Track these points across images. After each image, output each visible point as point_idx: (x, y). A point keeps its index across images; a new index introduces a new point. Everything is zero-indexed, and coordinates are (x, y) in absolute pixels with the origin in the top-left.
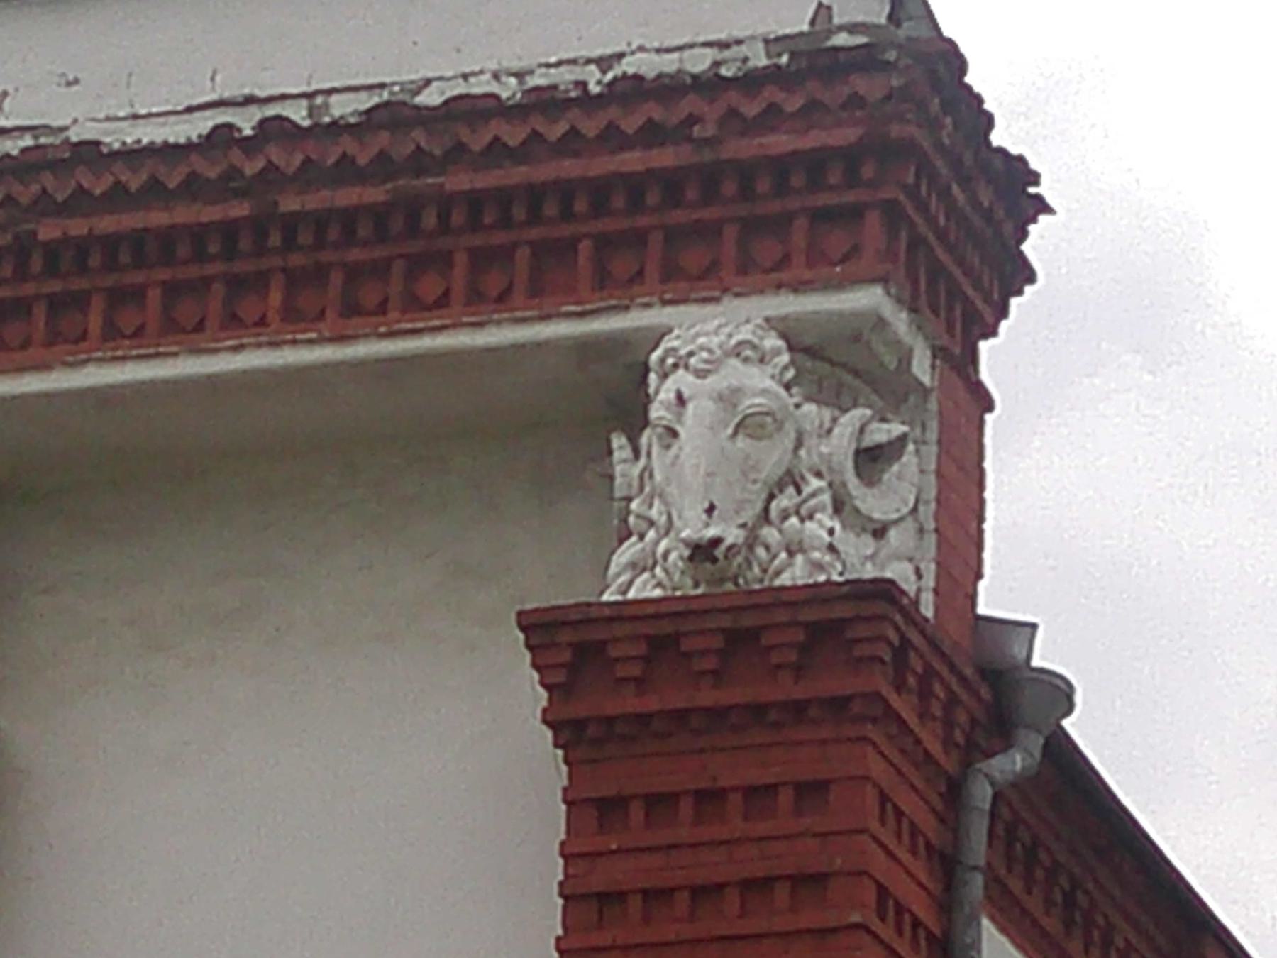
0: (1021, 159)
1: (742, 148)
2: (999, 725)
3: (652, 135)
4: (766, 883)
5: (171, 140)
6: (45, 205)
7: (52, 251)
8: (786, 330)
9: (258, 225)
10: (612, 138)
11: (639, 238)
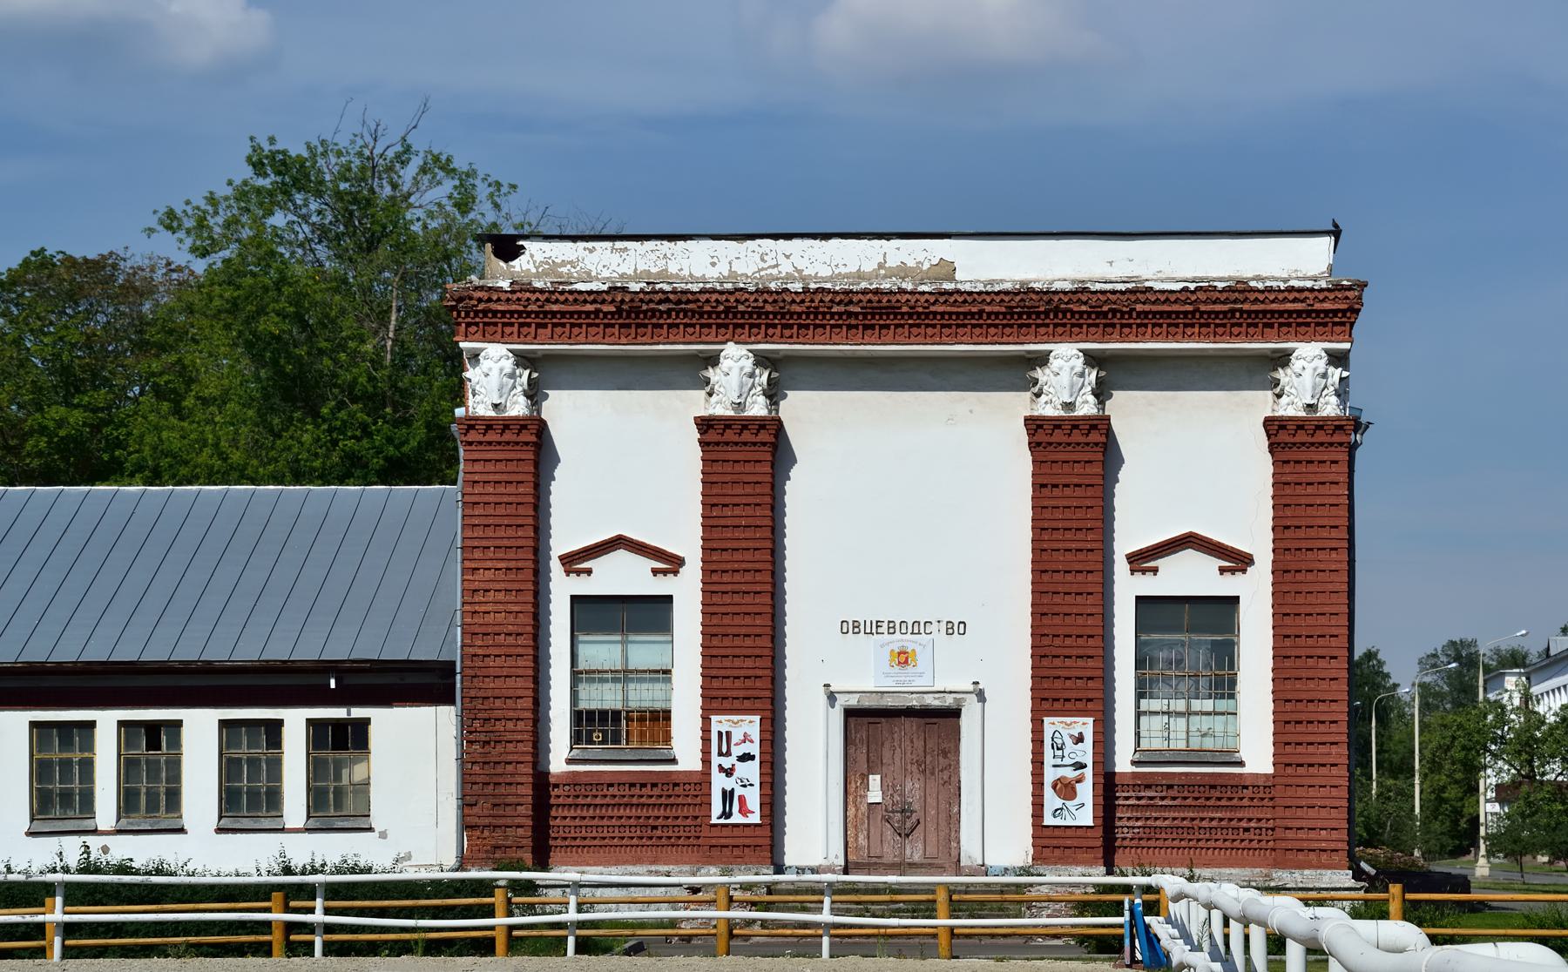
0: (39, 263)
1: (1317, 306)
2: (41, 763)
3: (1295, 300)
4: (1288, 462)
5: (911, 263)
6: (1137, 301)
7: (1139, 314)
8: (1326, 351)
9: (1193, 313)
10: (1285, 300)
11: (1080, 326)
